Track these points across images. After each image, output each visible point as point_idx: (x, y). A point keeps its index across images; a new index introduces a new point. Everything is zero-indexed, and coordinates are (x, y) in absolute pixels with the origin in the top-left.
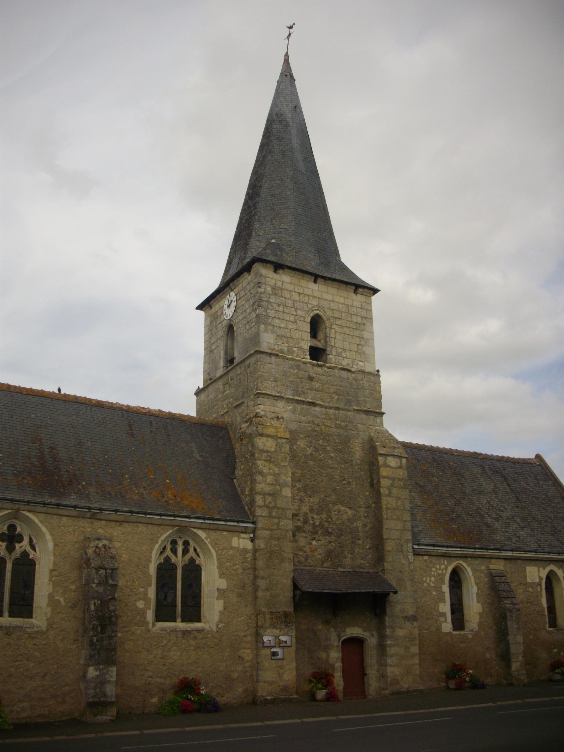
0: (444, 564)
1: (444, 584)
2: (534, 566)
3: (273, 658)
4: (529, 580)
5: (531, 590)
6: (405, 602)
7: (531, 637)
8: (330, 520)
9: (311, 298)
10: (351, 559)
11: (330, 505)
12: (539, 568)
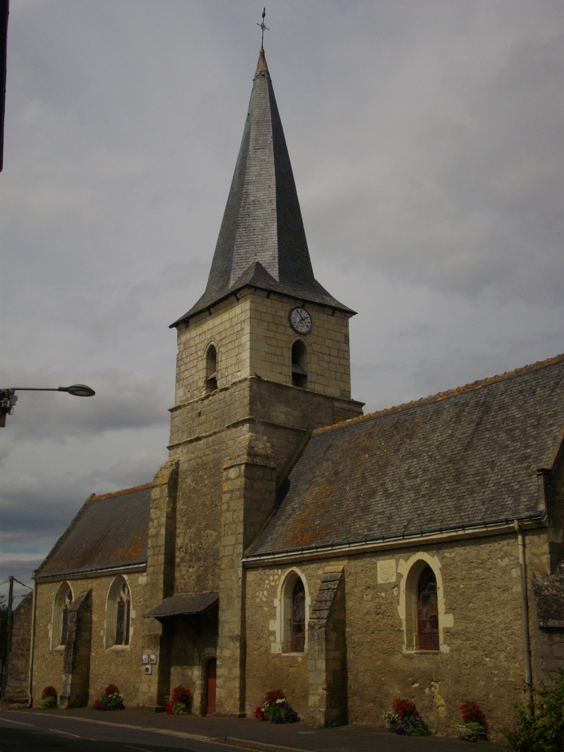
0: (278, 574)
1: (276, 597)
2: (390, 559)
3: (146, 673)
4: (380, 581)
5: (383, 594)
6: (232, 622)
7: (379, 663)
8: (201, 546)
9: (280, 323)
10: (212, 580)
11: (202, 532)
12: (397, 561)
